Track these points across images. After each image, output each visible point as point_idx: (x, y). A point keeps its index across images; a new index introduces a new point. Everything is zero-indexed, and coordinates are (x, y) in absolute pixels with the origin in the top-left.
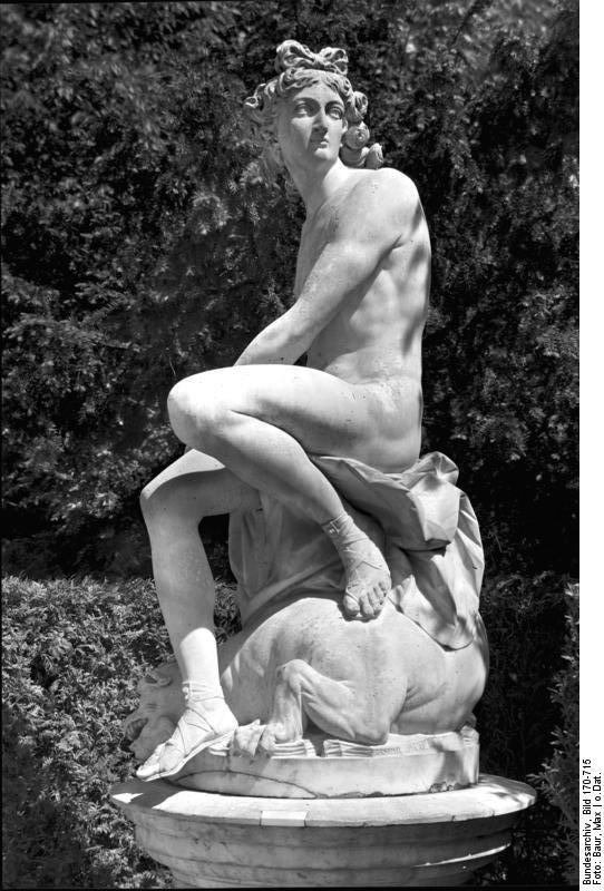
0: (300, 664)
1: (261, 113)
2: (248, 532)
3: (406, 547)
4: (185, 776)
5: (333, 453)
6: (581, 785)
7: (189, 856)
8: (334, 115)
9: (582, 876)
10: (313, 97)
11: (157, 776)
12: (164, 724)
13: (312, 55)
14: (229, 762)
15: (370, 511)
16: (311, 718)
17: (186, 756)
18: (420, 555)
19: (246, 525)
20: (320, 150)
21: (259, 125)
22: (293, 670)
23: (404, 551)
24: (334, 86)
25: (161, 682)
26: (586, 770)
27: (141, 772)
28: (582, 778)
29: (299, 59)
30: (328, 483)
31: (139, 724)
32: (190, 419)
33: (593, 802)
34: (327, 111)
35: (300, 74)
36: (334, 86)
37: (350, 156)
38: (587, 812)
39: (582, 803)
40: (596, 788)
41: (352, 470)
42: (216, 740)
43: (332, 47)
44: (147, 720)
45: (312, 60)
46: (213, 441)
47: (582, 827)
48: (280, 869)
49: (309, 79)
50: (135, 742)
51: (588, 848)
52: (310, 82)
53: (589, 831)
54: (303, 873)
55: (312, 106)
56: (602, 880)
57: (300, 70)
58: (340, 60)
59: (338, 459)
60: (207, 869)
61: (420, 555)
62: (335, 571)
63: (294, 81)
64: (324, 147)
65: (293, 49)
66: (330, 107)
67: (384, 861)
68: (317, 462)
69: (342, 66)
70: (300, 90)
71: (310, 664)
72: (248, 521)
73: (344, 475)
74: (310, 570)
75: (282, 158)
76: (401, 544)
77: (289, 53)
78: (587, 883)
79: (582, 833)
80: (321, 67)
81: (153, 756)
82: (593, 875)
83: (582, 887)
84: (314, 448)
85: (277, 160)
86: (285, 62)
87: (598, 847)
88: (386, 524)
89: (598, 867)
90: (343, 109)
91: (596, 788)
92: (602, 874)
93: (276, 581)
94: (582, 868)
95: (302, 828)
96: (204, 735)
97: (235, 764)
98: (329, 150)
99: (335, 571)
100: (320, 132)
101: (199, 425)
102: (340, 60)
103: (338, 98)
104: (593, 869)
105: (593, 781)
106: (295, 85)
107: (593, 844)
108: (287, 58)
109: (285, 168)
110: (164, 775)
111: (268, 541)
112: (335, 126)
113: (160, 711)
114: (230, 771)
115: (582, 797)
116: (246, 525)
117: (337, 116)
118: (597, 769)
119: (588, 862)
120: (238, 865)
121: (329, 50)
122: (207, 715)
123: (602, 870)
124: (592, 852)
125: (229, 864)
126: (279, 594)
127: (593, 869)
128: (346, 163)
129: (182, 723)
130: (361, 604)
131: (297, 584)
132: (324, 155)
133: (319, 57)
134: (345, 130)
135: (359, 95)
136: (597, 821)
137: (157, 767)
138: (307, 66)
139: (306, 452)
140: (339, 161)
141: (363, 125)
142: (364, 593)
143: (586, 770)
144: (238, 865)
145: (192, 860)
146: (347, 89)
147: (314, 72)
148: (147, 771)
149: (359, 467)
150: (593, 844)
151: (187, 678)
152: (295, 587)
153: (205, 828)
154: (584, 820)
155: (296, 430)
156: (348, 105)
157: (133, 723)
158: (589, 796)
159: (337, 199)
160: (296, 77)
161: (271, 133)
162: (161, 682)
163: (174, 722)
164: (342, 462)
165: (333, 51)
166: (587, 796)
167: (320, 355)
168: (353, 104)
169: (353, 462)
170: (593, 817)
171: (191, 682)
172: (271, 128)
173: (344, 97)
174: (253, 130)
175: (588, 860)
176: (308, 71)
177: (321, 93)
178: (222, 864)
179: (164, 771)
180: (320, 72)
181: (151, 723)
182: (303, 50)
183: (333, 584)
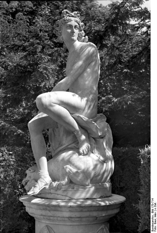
0: (68, 166)
1: (58, 28)
2: (54, 133)
3: (93, 137)
4: (39, 195)
5: (76, 114)
6: (151, 205)
7: (40, 214)
8: (76, 29)
9: (151, 229)
10: (71, 24)
11: (33, 194)
12: (33, 182)
13: (71, 13)
14: (50, 190)
15: (86, 128)
16: (71, 179)
17: (40, 189)
18: (98, 139)
19: (54, 131)
20: (73, 38)
21: (57, 31)
22: (66, 168)
23: (93, 138)
24: (76, 21)
25: (32, 171)
26: (153, 201)
27: (28, 193)
28: (151, 203)
29: (68, 14)
30: (73, 119)
31: (27, 181)
32: (42, 104)
33: (154, 210)
34: (75, 27)
35: (68, 18)
36: (76, 21)
37: (79, 38)
38: (153, 212)
39: (151, 210)
40: (155, 206)
41: (81, 118)
42: (47, 185)
43: (76, 11)
44: (29, 180)
45: (71, 15)
46: (46, 109)
47: (151, 216)
48: (64, 217)
49: (71, 19)
50: (25, 186)
51: (153, 222)
52: (71, 20)
53: (153, 217)
54: (69, 218)
55: (71, 27)
56: (156, 230)
57: (68, 17)
58: (78, 15)
59: (78, 115)
60: (45, 217)
61: (98, 139)
62: (77, 143)
63: (67, 20)
64: (74, 37)
65: (66, 12)
66: (75, 27)
67: (89, 215)
68: (73, 116)
69: (78, 16)
70: (68, 22)
71: (71, 166)
72: (54, 131)
73: (79, 119)
74: (70, 143)
75: (63, 39)
76: (93, 136)
77: (65, 13)
78: (152, 231)
79: (151, 218)
80: (73, 16)
81: (31, 189)
82: (154, 229)
83: (151, 232)
84: (72, 113)
85: (62, 40)
86: (64, 15)
87: (155, 222)
88: (89, 132)
89: (155, 227)
90: (78, 27)
91: (155, 206)
92: (156, 229)
93: (62, 145)
94: (151, 227)
95: (69, 207)
96: (44, 184)
97: (52, 191)
98: (75, 38)
99: (77, 143)
100: (73, 32)
101: (44, 106)
102: (78, 15)
103: (78, 25)
104: (154, 227)
105: (154, 204)
106: (67, 21)
107: (154, 221)
108: (65, 14)
109: (63, 42)
110: (34, 194)
111: (57, 134)
112: (76, 31)
113: (32, 178)
114: (50, 193)
115: (151, 208)
116: (54, 131)
117: (77, 29)
118: (155, 201)
119: (153, 226)
120: (53, 217)
121: (75, 12)
122: (45, 179)
123: (156, 227)
124: (154, 223)
125: (51, 216)
126: (62, 149)
127: (154, 227)
128: (79, 41)
129: (39, 181)
130: (83, 151)
131: (67, 146)
132: (74, 39)
133: (73, 14)
134: (79, 32)
135: (83, 24)
136: (155, 215)
137: (32, 192)
138: (70, 16)
139: (70, 114)
140: (77, 40)
141: (83, 31)
142: (84, 149)
143: (153, 201)
144: (53, 217)
145: (41, 215)
146: (79, 22)
147: (71, 18)
148: (30, 193)
149: (84, 118)
150: (154, 221)
151: (40, 169)
152: (66, 147)
153: (44, 207)
154: (152, 214)
155: (67, 108)
156: (80, 26)
157: (25, 181)
158: (153, 208)
159: (77, 50)
160: (67, 19)
161: (60, 33)
162: (32, 171)
163: (36, 181)
164: (79, 116)
165: (76, 12)
166: (152, 208)
167: (72, 89)
168: (81, 26)
169: (81, 116)
170: (154, 214)
171: (41, 171)
172: (60, 32)
173: (79, 24)
174: (56, 32)
175: (153, 225)
176: (70, 17)
177: (73, 23)
178: (49, 216)
179: (34, 193)
180: (73, 18)
181: (30, 181)
182: (69, 12)
183: (76, 146)
